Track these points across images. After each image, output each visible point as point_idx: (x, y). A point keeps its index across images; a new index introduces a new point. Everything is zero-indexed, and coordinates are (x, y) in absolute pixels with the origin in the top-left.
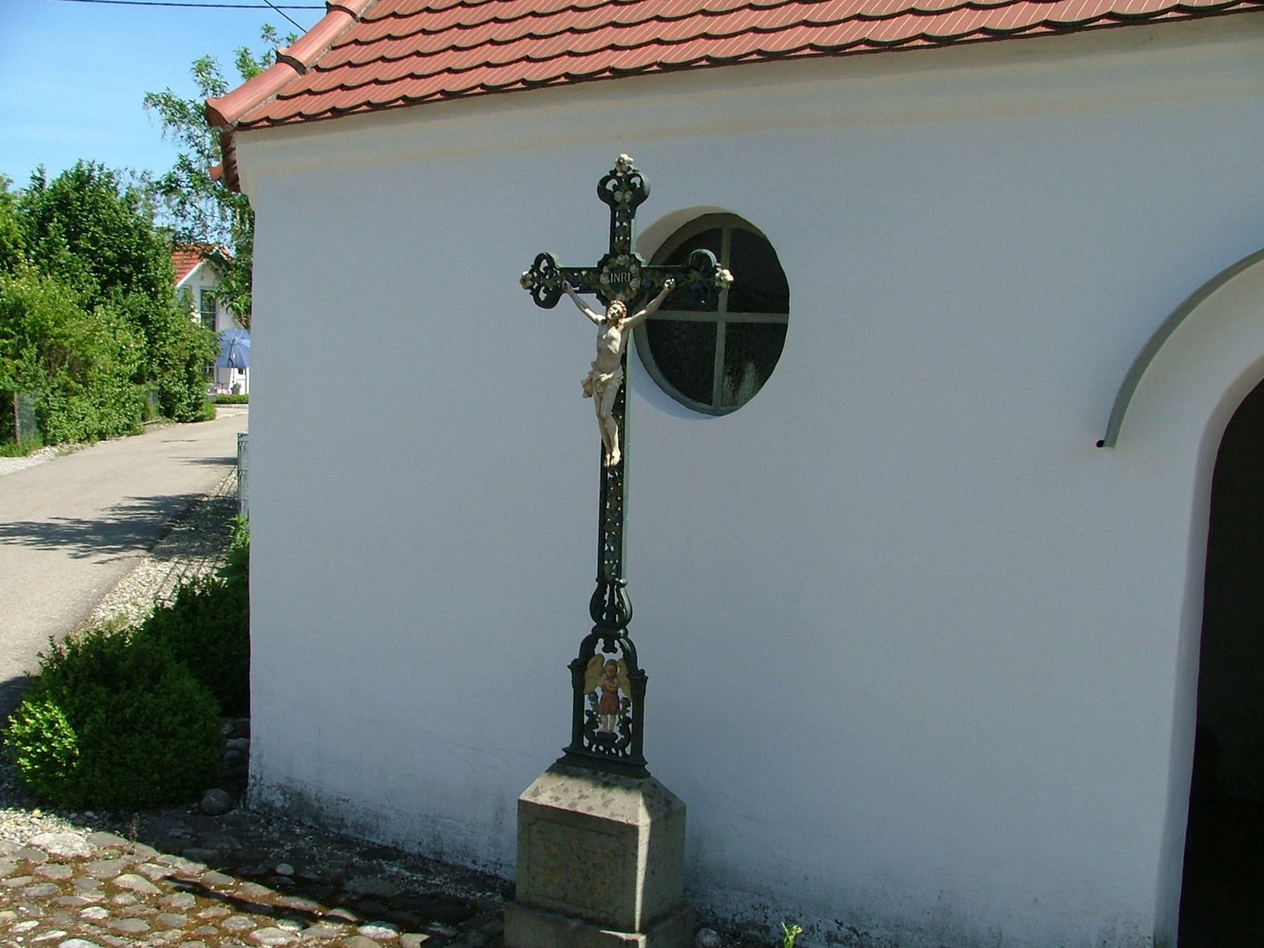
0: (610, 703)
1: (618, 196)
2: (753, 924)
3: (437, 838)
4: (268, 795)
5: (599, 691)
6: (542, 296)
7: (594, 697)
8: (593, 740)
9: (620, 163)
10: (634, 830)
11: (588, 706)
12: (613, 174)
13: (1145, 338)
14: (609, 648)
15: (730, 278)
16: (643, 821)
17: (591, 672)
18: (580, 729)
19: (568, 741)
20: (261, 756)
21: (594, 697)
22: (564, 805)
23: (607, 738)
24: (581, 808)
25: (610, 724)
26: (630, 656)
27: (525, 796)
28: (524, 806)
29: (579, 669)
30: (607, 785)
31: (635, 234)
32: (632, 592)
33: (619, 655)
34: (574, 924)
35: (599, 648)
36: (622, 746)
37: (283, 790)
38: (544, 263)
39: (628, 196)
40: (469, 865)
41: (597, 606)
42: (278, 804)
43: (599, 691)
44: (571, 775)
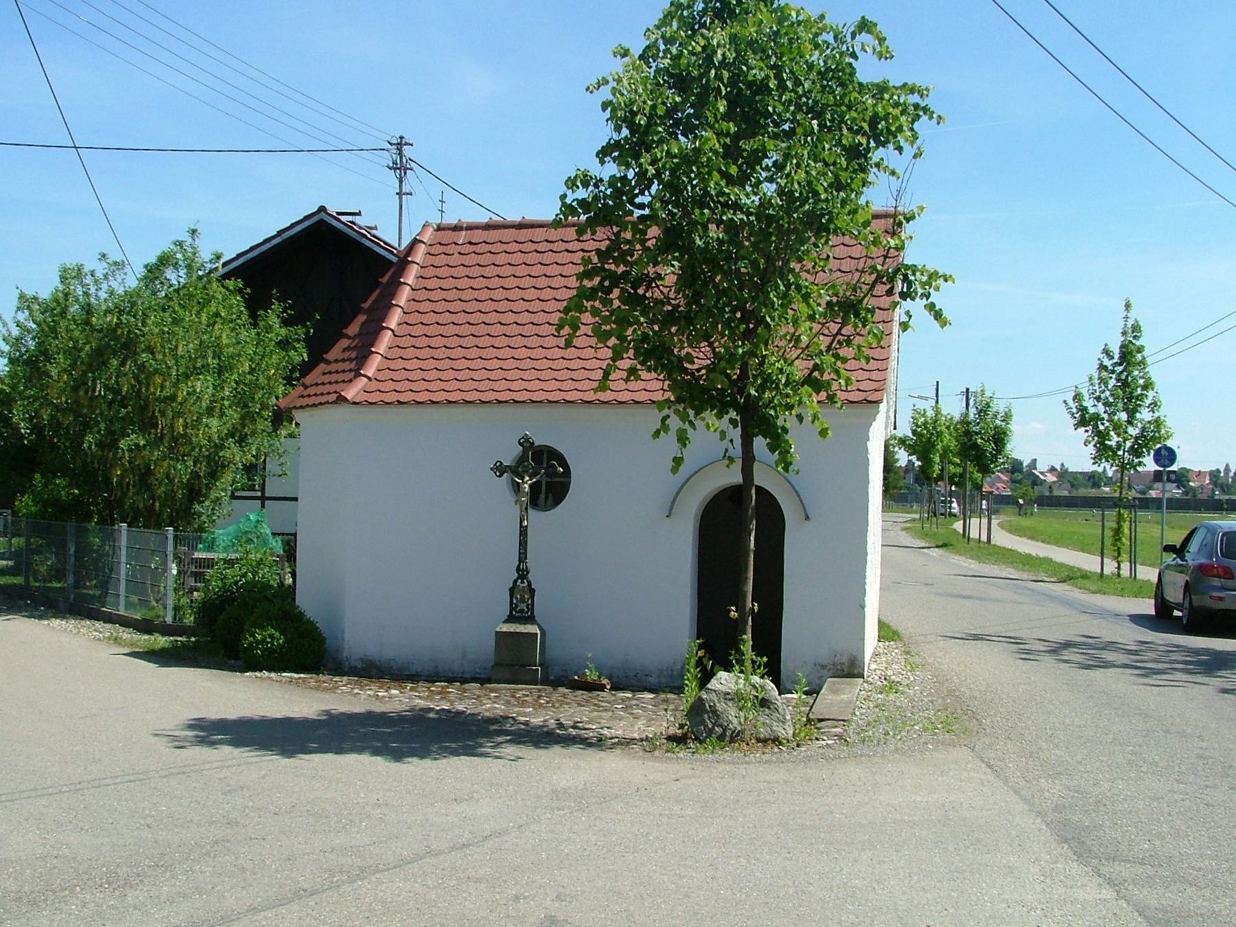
0: (523, 600)
1: (525, 444)
2: (562, 676)
3: (437, 667)
4: (353, 663)
5: (519, 597)
6: (498, 474)
7: (517, 599)
8: (517, 612)
9: (526, 435)
10: (536, 634)
11: (515, 601)
12: (523, 438)
13: (692, 473)
14: (522, 582)
15: (562, 470)
16: (539, 632)
17: (515, 591)
18: (511, 609)
19: (508, 613)
20: (350, 648)
21: (517, 599)
22: (512, 630)
23: (522, 611)
24: (518, 631)
25: (523, 606)
26: (529, 584)
27: (498, 630)
28: (497, 632)
29: (512, 590)
30: (525, 624)
31: (1014, 575)
32: (530, 562)
33: (526, 584)
34: (516, 667)
35: (518, 583)
36: (527, 612)
37: (362, 660)
38: (498, 464)
39: (528, 445)
40: (450, 675)
41: (518, 569)
42: (359, 666)
43: (519, 597)
44: (512, 623)
